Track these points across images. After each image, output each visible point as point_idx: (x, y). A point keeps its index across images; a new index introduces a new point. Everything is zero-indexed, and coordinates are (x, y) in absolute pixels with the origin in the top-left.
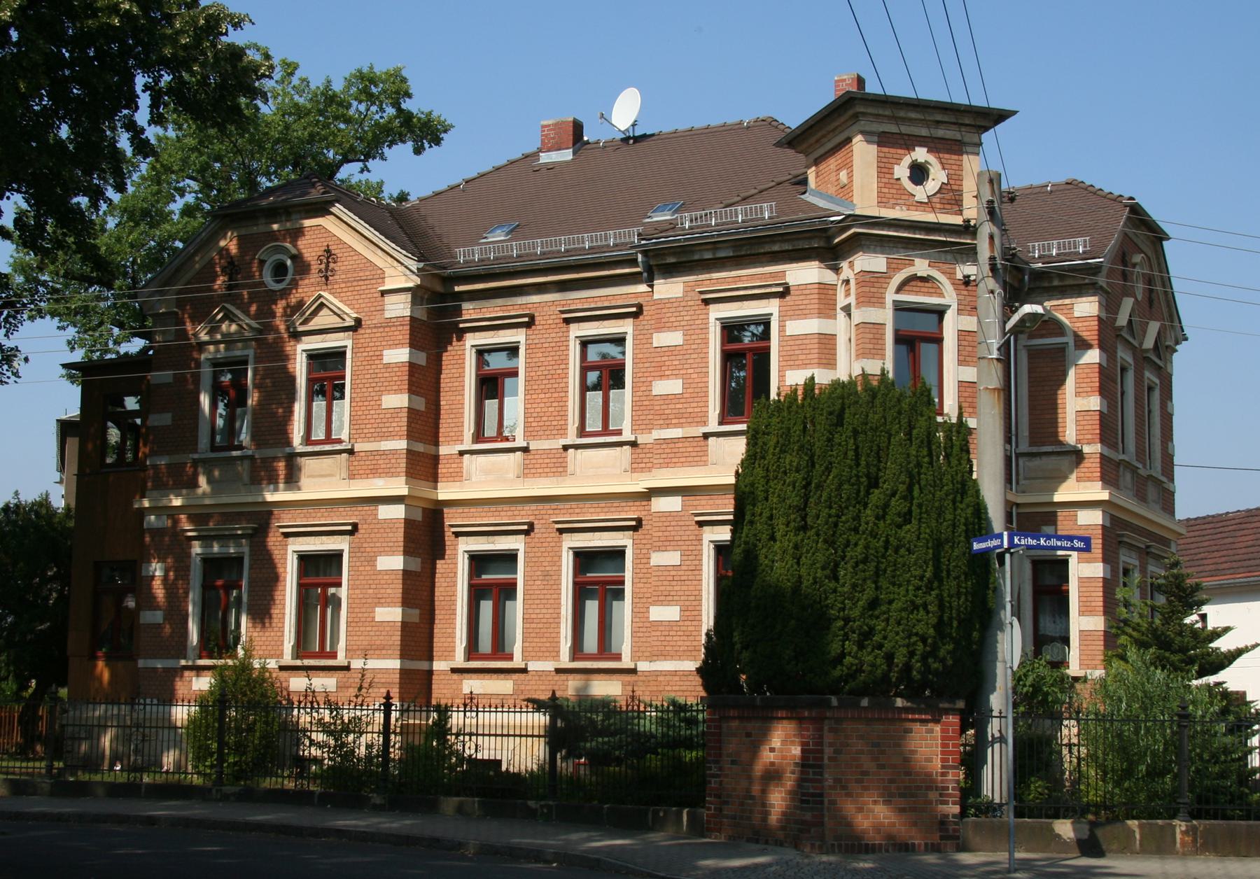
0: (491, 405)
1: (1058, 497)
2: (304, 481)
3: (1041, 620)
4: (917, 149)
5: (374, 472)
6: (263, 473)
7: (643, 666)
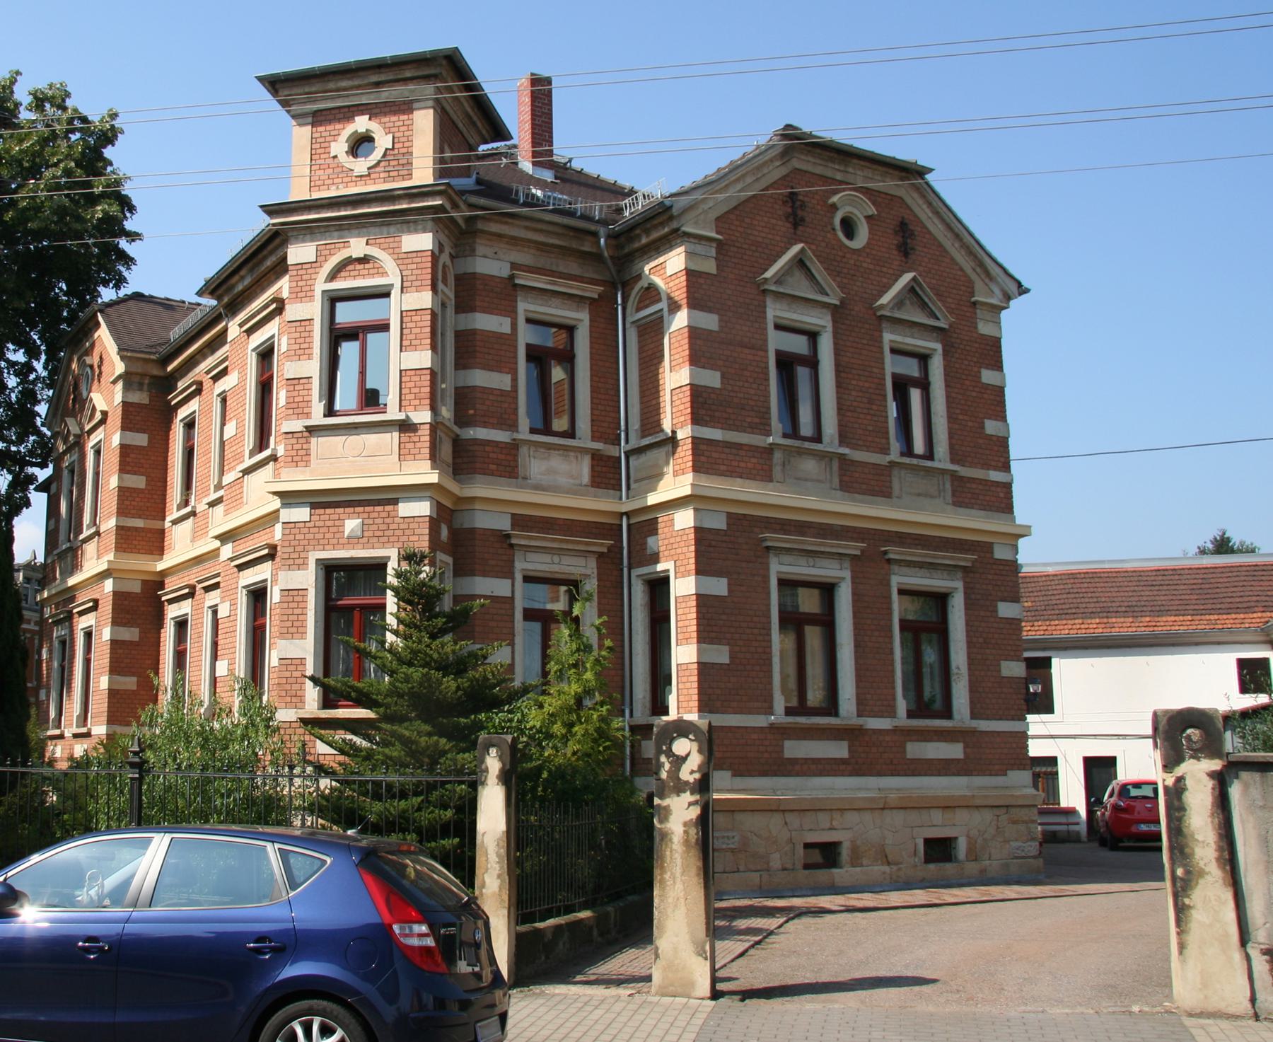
1: (652, 499)
4: (356, 118)
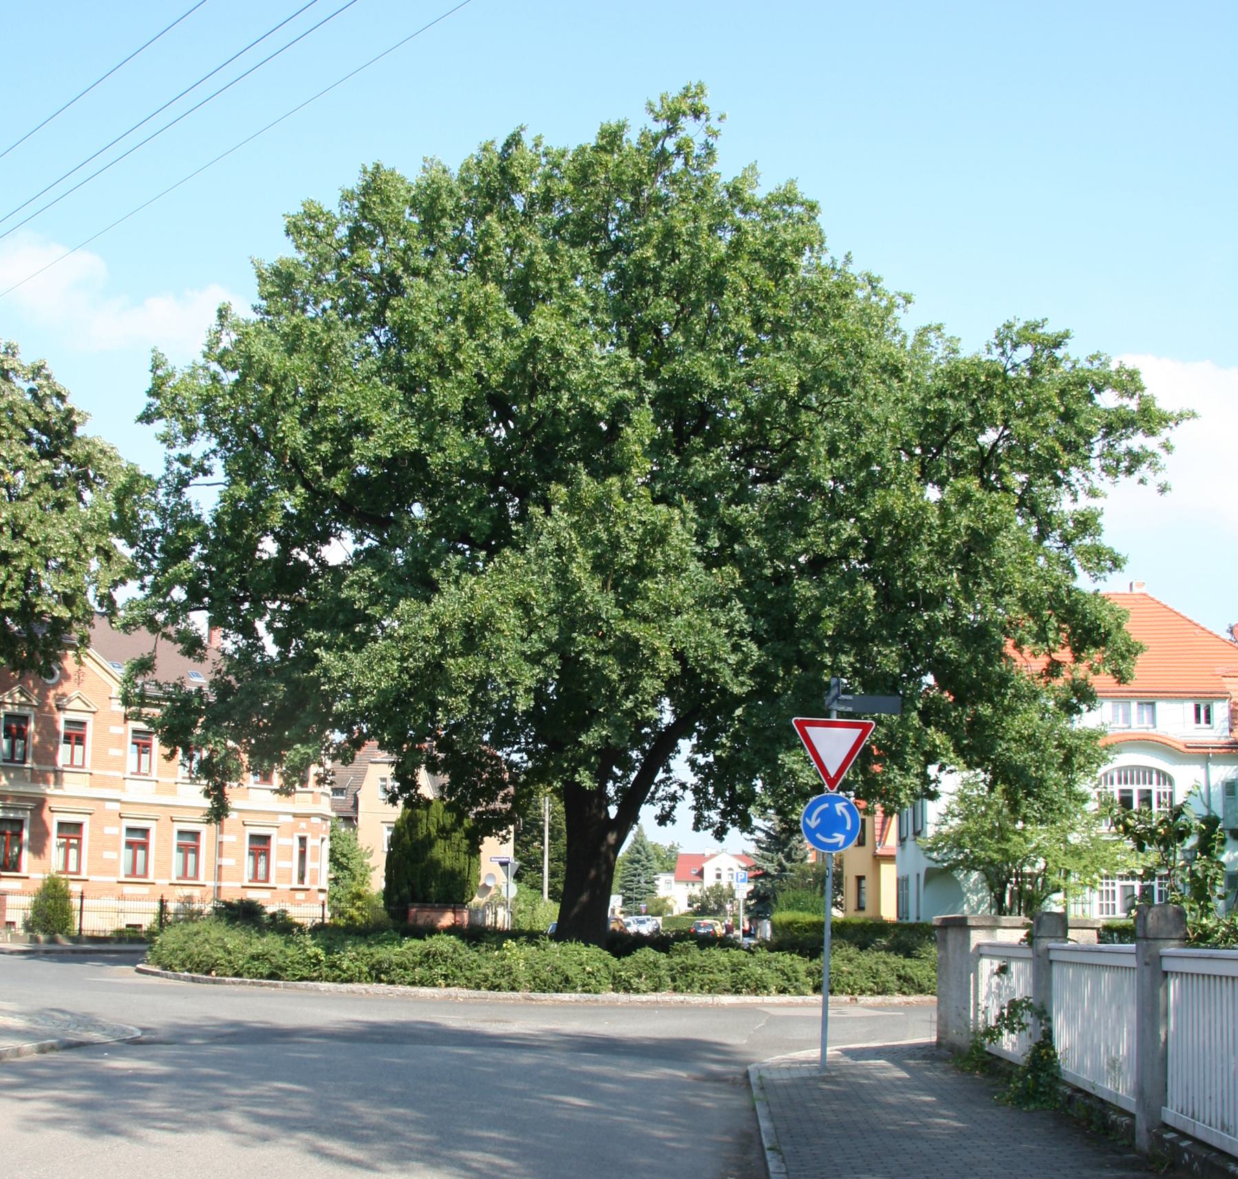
0: (145, 757)
2: (65, 785)
3: (1124, 1044)
5: (102, 785)
6: (38, 777)
7: (91, 878)
